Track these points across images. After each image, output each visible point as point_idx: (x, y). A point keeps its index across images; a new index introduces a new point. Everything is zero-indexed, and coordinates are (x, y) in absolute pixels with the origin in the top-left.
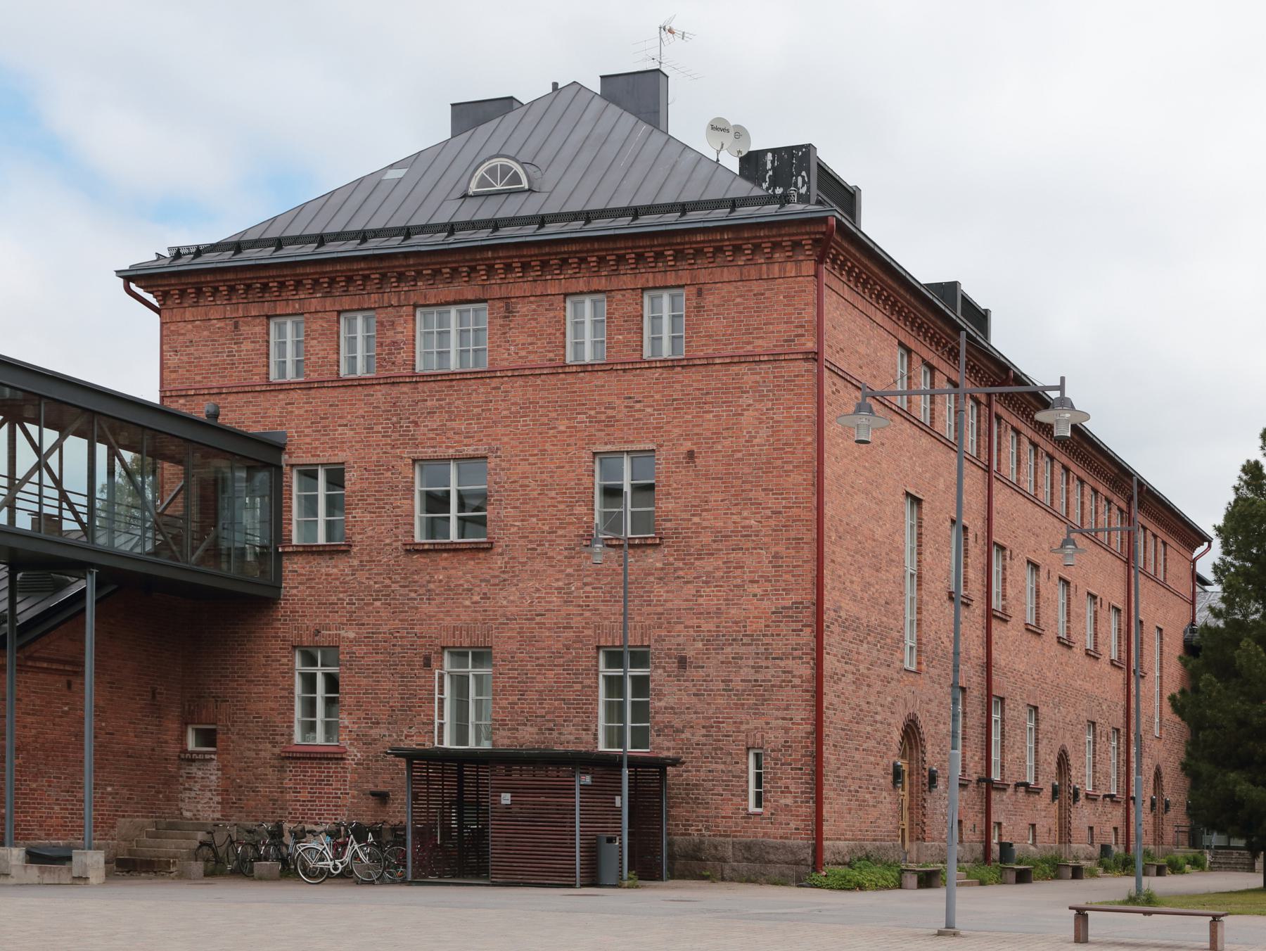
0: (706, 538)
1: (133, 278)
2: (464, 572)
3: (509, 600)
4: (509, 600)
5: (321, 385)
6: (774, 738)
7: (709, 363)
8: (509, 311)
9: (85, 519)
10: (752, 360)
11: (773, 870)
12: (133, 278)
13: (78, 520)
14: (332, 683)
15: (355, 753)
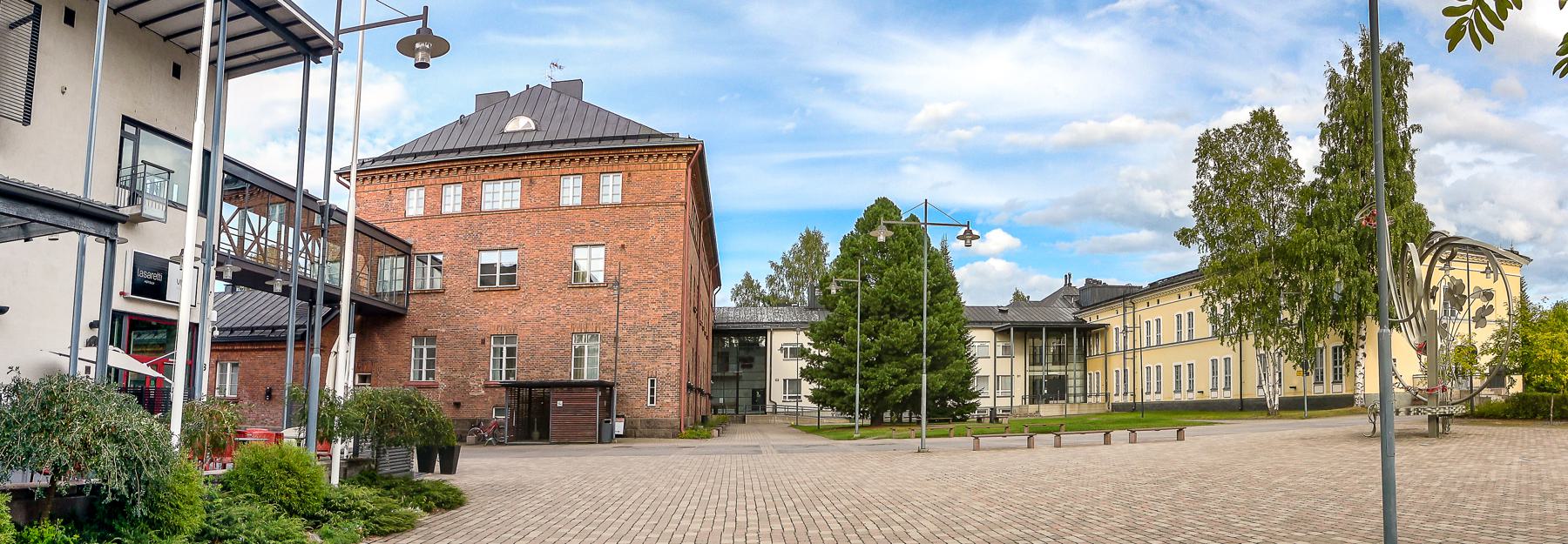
0: (629, 283)
1: (747, 275)
2: (505, 300)
3: (527, 312)
4: (527, 312)
5: (432, 217)
6: (662, 372)
7: (634, 205)
8: (532, 182)
9: (235, 239)
10: (656, 204)
11: (662, 432)
12: (747, 275)
13: (232, 244)
14: (431, 353)
15: (443, 385)
